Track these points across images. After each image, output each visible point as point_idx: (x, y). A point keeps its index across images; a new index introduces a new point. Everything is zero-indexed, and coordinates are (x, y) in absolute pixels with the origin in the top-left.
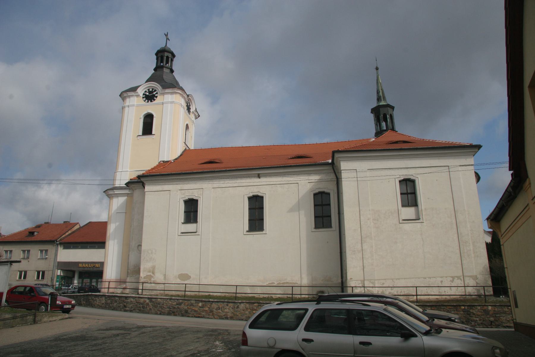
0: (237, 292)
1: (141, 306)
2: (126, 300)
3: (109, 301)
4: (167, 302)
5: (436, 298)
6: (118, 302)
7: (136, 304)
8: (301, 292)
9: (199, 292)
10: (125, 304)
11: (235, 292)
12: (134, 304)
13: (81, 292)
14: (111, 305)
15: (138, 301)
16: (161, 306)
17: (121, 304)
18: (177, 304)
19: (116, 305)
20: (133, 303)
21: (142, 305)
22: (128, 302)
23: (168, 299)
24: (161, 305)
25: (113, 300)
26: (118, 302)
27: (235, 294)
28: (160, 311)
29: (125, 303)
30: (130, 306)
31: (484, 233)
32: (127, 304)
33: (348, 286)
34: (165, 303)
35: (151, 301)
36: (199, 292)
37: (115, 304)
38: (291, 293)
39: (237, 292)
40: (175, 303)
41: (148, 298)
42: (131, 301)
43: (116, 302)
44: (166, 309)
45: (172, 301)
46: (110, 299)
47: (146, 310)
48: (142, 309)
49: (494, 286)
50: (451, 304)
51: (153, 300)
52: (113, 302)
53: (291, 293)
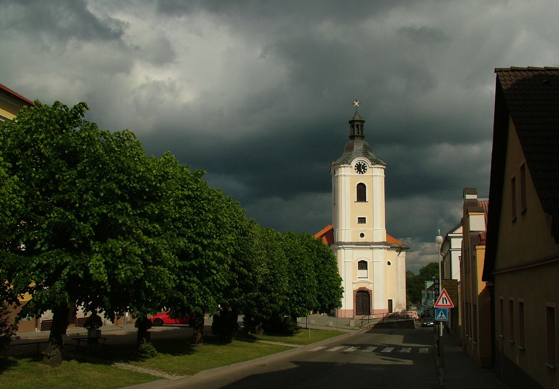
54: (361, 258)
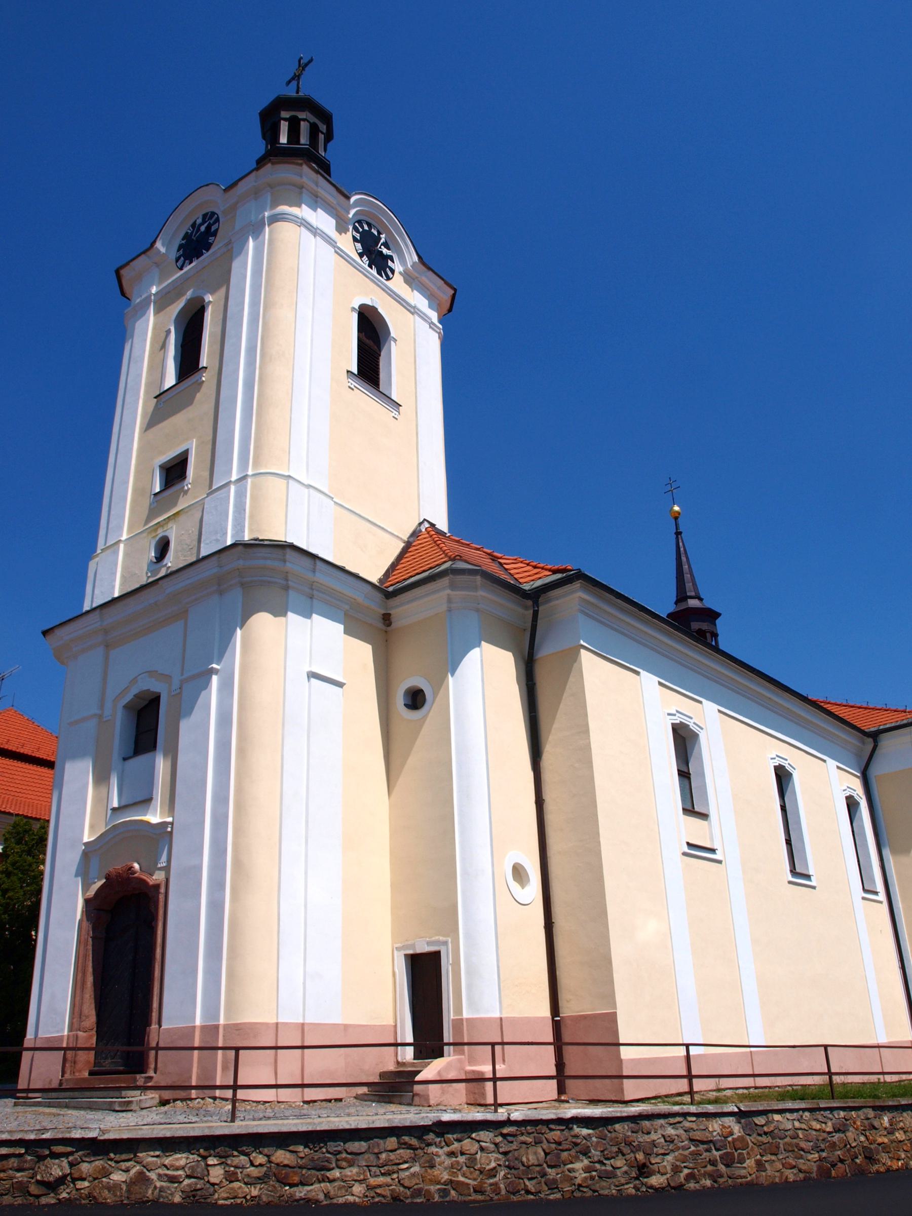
0: (684, 1072)
1: (717, 1154)
2: (642, 1138)
3: (533, 1156)
4: (804, 1126)
5: (861, 1081)
6: (595, 1154)
7: (693, 1148)
8: (303, 1078)
9: (303, 1086)
10: (640, 1156)
11: (833, 1070)
12: (684, 1148)
13: (18, 1095)
14: (551, 1172)
15: (698, 1135)
16: (790, 1144)
17: (619, 1162)
18: (837, 1130)
19: (587, 1170)
20: (678, 1148)
21: (717, 1150)
22: (654, 1144)
23: (804, 1110)
24: (788, 1140)
25: (559, 1144)
26: (595, 1154)
27: (685, 1081)
28: (794, 1167)
29: (638, 1149)
30: (665, 1163)
31: (329, 166)
32: (647, 1155)
33: (621, 1042)
34: (801, 1129)
35: (750, 1129)
36: (303, 1086)
37: (578, 1165)
38: (498, 1083)
39: (684, 1072)
40: (829, 1128)
41: (740, 1115)
42: (669, 1140)
43: (586, 1153)
44: (810, 1157)
45: (818, 1115)
46: (538, 1142)
47: (743, 1172)
48: (722, 1167)
49: (139, 1048)
50: (722, 1108)
51: (760, 1120)
52: (565, 1155)
53: (498, 1083)
54: (134, 681)
